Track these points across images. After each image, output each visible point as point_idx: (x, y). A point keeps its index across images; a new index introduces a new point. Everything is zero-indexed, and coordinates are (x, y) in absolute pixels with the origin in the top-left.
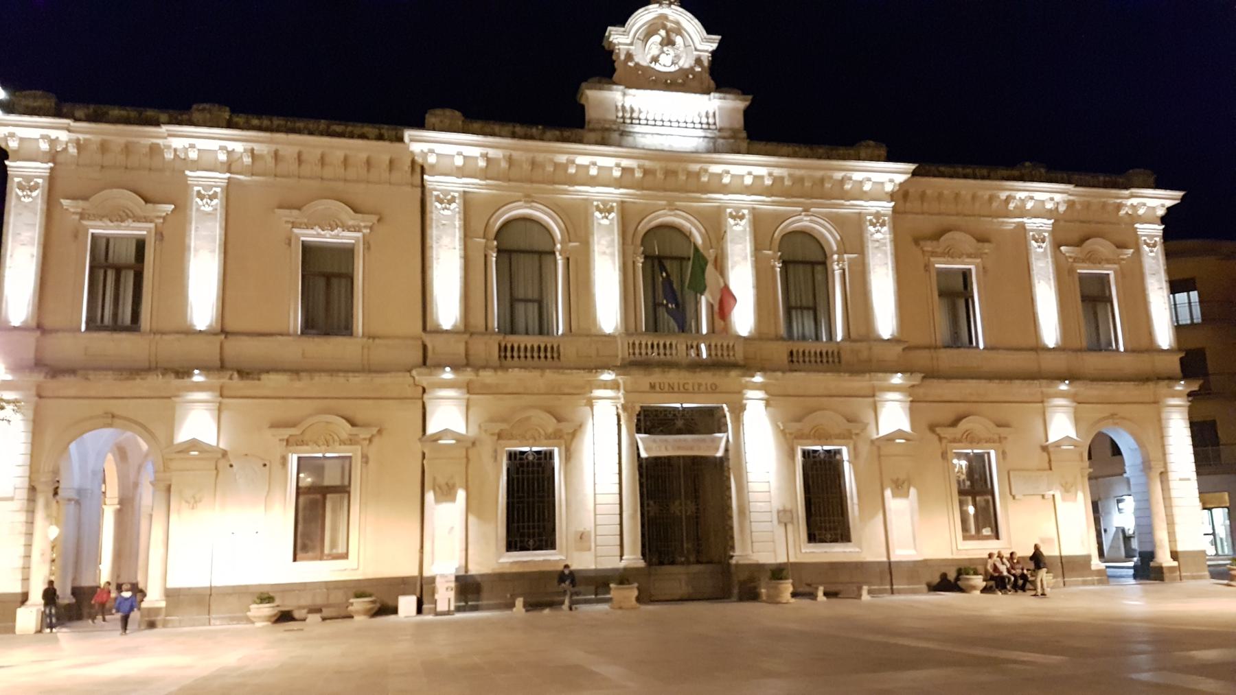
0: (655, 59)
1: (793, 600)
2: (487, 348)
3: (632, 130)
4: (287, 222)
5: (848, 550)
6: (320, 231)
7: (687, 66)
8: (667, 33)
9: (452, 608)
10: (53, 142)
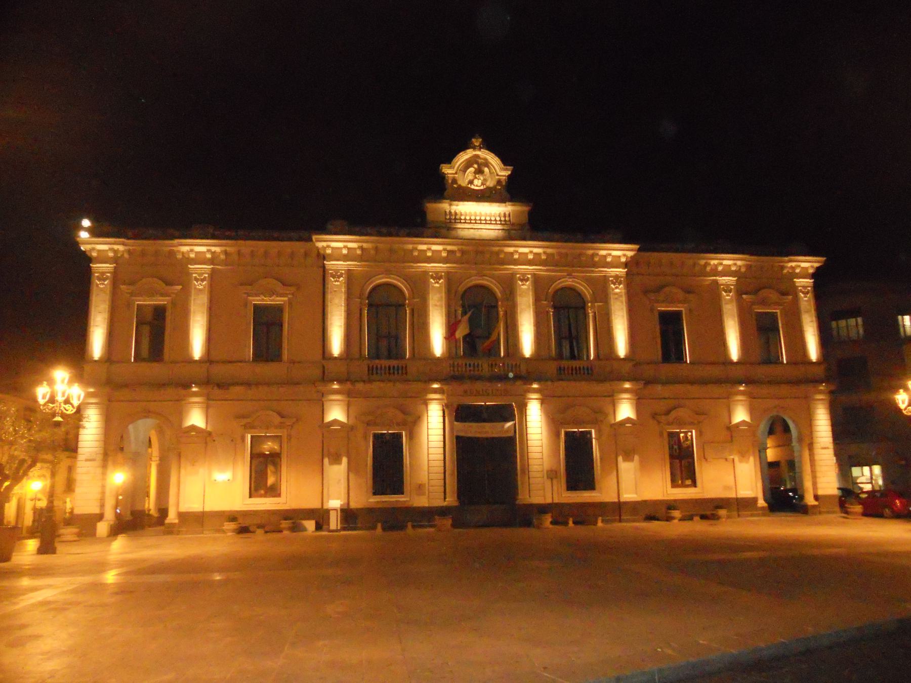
0: (471, 182)
1: (551, 526)
2: (361, 368)
3: (455, 226)
4: (245, 293)
5: (593, 494)
6: (264, 297)
7: (491, 185)
8: (479, 166)
9: (339, 528)
10: (115, 251)
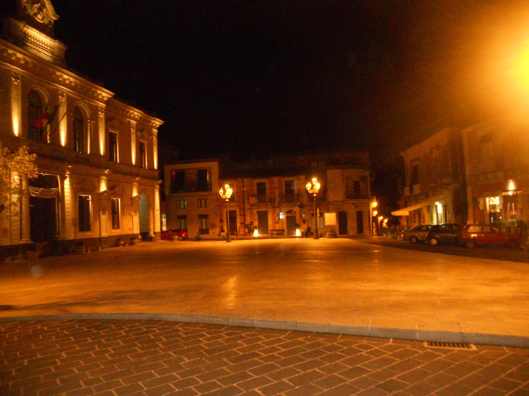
0: (36, 15)
5: (90, 234)
